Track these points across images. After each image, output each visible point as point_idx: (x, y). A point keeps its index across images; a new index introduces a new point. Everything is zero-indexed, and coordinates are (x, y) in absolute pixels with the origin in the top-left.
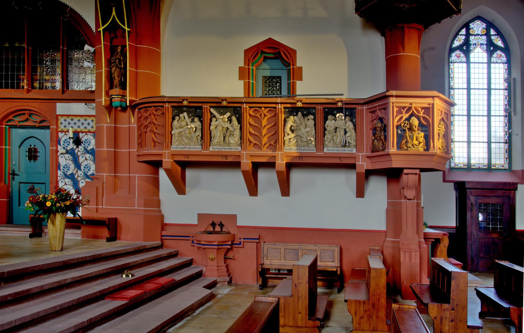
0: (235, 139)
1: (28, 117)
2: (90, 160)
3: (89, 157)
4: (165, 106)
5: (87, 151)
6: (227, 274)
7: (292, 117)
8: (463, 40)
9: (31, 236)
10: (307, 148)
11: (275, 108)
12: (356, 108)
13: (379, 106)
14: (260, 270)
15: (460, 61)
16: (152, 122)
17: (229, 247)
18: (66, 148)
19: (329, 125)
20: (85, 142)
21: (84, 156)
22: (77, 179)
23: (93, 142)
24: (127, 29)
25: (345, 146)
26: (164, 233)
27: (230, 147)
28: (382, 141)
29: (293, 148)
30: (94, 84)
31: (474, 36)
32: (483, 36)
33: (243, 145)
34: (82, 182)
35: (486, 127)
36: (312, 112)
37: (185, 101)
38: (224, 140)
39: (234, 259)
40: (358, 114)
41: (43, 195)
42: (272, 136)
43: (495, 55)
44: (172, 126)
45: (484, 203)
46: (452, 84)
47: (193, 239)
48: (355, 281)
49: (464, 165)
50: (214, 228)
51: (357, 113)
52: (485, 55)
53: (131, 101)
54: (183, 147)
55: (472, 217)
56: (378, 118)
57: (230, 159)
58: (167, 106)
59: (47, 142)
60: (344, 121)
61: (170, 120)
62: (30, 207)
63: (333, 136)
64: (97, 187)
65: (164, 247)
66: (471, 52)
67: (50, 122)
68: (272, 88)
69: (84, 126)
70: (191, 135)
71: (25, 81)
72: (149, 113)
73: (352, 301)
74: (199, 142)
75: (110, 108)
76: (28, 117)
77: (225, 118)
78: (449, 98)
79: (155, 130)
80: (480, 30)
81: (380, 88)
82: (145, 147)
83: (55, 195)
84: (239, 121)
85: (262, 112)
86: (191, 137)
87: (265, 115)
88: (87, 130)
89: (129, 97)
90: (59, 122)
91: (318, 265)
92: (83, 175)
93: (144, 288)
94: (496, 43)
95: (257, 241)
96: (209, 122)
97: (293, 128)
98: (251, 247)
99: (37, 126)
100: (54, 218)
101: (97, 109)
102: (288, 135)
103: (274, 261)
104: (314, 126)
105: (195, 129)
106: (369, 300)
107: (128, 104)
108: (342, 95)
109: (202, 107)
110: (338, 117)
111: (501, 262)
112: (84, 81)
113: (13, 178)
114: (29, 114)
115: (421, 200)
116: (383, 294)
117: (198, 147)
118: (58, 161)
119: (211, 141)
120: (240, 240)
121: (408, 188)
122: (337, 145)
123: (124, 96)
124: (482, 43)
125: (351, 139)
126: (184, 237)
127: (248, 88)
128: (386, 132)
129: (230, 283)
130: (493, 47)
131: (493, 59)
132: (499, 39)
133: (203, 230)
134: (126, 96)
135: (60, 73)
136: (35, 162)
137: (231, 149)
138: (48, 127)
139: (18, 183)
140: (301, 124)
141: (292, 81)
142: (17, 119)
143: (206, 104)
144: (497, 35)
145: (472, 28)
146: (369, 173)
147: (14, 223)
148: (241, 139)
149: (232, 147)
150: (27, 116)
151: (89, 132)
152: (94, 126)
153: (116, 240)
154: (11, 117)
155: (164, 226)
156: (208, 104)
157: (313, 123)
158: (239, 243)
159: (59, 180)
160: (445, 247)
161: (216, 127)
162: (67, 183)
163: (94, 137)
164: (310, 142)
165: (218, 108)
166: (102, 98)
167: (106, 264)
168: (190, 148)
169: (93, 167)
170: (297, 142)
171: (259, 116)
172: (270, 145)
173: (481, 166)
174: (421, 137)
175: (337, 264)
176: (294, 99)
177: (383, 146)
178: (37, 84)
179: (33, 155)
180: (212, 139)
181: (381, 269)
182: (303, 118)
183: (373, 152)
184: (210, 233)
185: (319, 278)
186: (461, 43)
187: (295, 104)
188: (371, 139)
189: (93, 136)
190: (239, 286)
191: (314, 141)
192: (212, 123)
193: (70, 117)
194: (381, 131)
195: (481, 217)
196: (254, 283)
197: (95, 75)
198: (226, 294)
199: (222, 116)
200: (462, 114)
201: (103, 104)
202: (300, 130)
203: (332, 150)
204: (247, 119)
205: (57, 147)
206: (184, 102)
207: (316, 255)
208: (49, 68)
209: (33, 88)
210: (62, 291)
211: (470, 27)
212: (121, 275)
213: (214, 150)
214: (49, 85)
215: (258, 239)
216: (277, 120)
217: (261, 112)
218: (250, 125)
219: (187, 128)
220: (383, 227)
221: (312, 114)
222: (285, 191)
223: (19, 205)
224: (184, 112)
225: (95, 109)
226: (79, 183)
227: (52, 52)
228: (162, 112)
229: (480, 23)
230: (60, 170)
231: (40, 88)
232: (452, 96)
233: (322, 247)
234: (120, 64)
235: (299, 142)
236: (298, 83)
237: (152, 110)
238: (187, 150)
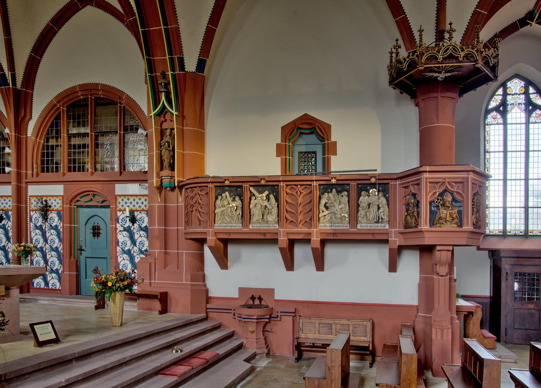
0: (272, 217)
1: (92, 198)
2: (144, 237)
3: (143, 234)
4: (209, 186)
5: (141, 229)
6: (265, 346)
7: (327, 194)
8: (500, 100)
9: (97, 308)
10: (341, 225)
11: (311, 185)
12: (389, 184)
13: (412, 181)
14: (296, 343)
15: (496, 123)
16: (197, 201)
17: (267, 320)
18: (123, 225)
19: (362, 202)
20: (139, 220)
21: (139, 233)
22: (133, 254)
23: (146, 220)
24: (175, 113)
25: (377, 222)
26: (209, 306)
27: (268, 225)
28: (415, 217)
29: (328, 225)
30: (146, 165)
31: (511, 96)
32: (521, 95)
33: (280, 222)
34: (138, 258)
35: (524, 175)
36: (346, 188)
37: (227, 181)
38: (262, 218)
39: (272, 332)
40: (391, 189)
41: (105, 276)
42: (308, 213)
43: (534, 115)
44: (215, 205)
45: (520, 273)
46: (487, 148)
47: (234, 312)
48: (387, 360)
49: (499, 232)
50: (254, 302)
51: (390, 188)
52: (523, 115)
53: (179, 182)
54: (225, 225)
55: (507, 287)
56: (411, 193)
57: (268, 237)
58: (211, 186)
59: (108, 220)
60: (377, 197)
61: (214, 200)
62: (95, 287)
63: (366, 212)
64: (150, 263)
65: (208, 319)
66: (508, 112)
67: (110, 203)
68: (308, 163)
69: (139, 205)
70: (232, 214)
71: (89, 164)
72: (194, 193)
73: (383, 386)
74: (239, 220)
75: (160, 188)
76: (92, 198)
77: (264, 196)
78: (485, 170)
79: (200, 209)
80: (518, 89)
81: (414, 163)
82: (192, 225)
83: (115, 275)
84: (277, 199)
85: (298, 189)
86: (233, 216)
87: (301, 193)
88: (141, 209)
89: (177, 178)
90: (118, 202)
91: (351, 340)
92: (138, 250)
93: (191, 363)
94: (535, 102)
95: (294, 315)
96: (248, 200)
97: (327, 205)
98: (288, 321)
99: (99, 206)
100: (114, 297)
101: (150, 188)
102: (323, 212)
103: (309, 335)
104: (347, 203)
105: (236, 208)
106: (400, 385)
107: (176, 185)
108: (376, 170)
109: (242, 186)
110: (372, 193)
111: (537, 344)
112: (138, 162)
113: (81, 254)
114: (93, 195)
115: (454, 275)
116: (414, 379)
117: (239, 225)
118: (117, 238)
119: (250, 219)
120: (277, 314)
121: (441, 264)
122: (370, 221)
123: (172, 177)
124: (520, 102)
125: (384, 215)
126: (227, 310)
127: (285, 165)
128: (419, 208)
129: (268, 354)
130: (531, 106)
131: (532, 119)
132: (538, 97)
133: (243, 303)
134: (174, 177)
135: (118, 155)
136: (98, 238)
137: (269, 227)
138: (108, 207)
139: (85, 258)
140: (335, 201)
141: (326, 142)
142: (83, 199)
143: (246, 183)
144: (537, 93)
145: (510, 87)
146: (401, 248)
147: (82, 294)
148: (278, 217)
149: (270, 225)
150: (91, 197)
151: (143, 210)
152: (147, 205)
153: (167, 313)
154: (78, 198)
155: (208, 299)
156: (248, 183)
157: (347, 199)
158: (276, 316)
159: (118, 255)
160: (478, 320)
161: (255, 206)
162: (125, 258)
163: (147, 215)
164: (344, 219)
165: (257, 187)
166: (153, 179)
167: (158, 340)
168: (231, 226)
169: (147, 244)
170: (331, 218)
171: (295, 194)
172: (306, 222)
173: (518, 233)
174: (455, 213)
175: (369, 338)
176: (328, 176)
177: (416, 222)
178: (98, 166)
179: (96, 232)
180: (252, 217)
181: (412, 355)
182: (337, 195)
183: (405, 228)
184: (250, 307)
185: (351, 351)
186: (498, 103)
187: (330, 180)
188: (403, 214)
189: (146, 214)
190: (276, 357)
191: (347, 218)
192: (252, 202)
193: (127, 197)
194: (414, 207)
195: (516, 286)
196: (289, 354)
197: (147, 156)
198: (264, 367)
199: (261, 195)
200: (498, 206)
201: (155, 185)
202: (334, 206)
203: (365, 226)
204: (283, 196)
205: (116, 225)
206: (226, 182)
207: (349, 334)
208: (108, 152)
209: (96, 170)
210: (121, 369)
211: (508, 86)
212: (171, 349)
213: (254, 228)
214: (108, 166)
215: (294, 313)
216: (312, 206)
217: (297, 190)
218: (287, 202)
219: (229, 207)
220: (415, 302)
221: (346, 191)
222: (320, 266)
223: (86, 278)
224: (226, 191)
225: (147, 189)
226: (135, 258)
227: (111, 137)
228: (207, 192)
229: (518, 82)
230: (119, 246)
231: (101, 171)
232: (488, 160)
233: (355, 322)
234: (169, 147)
235: (334, 219)
236: (333, 158)
237: (197, 190)
238: (229, 228)
